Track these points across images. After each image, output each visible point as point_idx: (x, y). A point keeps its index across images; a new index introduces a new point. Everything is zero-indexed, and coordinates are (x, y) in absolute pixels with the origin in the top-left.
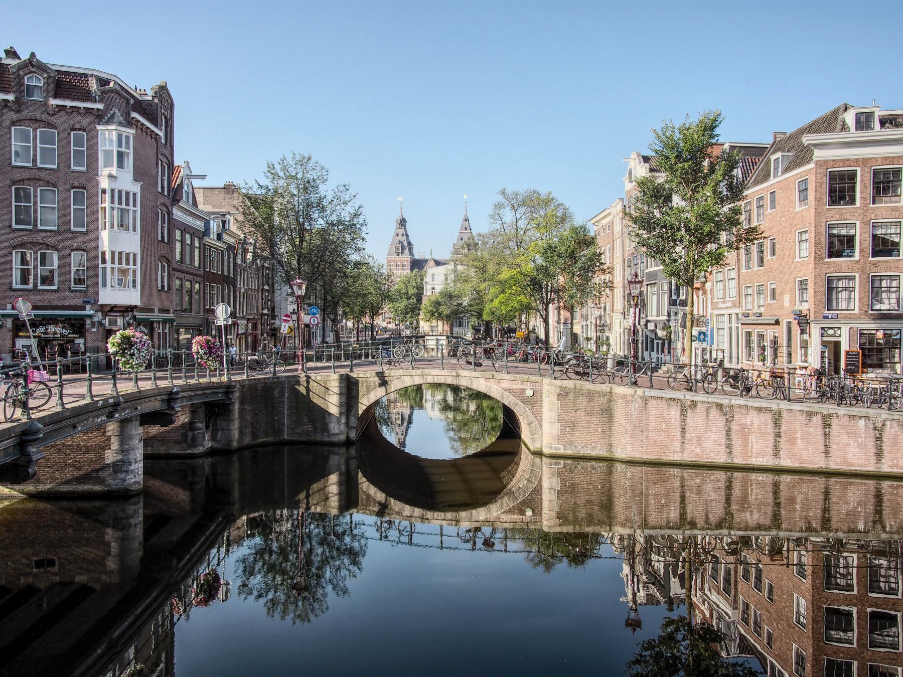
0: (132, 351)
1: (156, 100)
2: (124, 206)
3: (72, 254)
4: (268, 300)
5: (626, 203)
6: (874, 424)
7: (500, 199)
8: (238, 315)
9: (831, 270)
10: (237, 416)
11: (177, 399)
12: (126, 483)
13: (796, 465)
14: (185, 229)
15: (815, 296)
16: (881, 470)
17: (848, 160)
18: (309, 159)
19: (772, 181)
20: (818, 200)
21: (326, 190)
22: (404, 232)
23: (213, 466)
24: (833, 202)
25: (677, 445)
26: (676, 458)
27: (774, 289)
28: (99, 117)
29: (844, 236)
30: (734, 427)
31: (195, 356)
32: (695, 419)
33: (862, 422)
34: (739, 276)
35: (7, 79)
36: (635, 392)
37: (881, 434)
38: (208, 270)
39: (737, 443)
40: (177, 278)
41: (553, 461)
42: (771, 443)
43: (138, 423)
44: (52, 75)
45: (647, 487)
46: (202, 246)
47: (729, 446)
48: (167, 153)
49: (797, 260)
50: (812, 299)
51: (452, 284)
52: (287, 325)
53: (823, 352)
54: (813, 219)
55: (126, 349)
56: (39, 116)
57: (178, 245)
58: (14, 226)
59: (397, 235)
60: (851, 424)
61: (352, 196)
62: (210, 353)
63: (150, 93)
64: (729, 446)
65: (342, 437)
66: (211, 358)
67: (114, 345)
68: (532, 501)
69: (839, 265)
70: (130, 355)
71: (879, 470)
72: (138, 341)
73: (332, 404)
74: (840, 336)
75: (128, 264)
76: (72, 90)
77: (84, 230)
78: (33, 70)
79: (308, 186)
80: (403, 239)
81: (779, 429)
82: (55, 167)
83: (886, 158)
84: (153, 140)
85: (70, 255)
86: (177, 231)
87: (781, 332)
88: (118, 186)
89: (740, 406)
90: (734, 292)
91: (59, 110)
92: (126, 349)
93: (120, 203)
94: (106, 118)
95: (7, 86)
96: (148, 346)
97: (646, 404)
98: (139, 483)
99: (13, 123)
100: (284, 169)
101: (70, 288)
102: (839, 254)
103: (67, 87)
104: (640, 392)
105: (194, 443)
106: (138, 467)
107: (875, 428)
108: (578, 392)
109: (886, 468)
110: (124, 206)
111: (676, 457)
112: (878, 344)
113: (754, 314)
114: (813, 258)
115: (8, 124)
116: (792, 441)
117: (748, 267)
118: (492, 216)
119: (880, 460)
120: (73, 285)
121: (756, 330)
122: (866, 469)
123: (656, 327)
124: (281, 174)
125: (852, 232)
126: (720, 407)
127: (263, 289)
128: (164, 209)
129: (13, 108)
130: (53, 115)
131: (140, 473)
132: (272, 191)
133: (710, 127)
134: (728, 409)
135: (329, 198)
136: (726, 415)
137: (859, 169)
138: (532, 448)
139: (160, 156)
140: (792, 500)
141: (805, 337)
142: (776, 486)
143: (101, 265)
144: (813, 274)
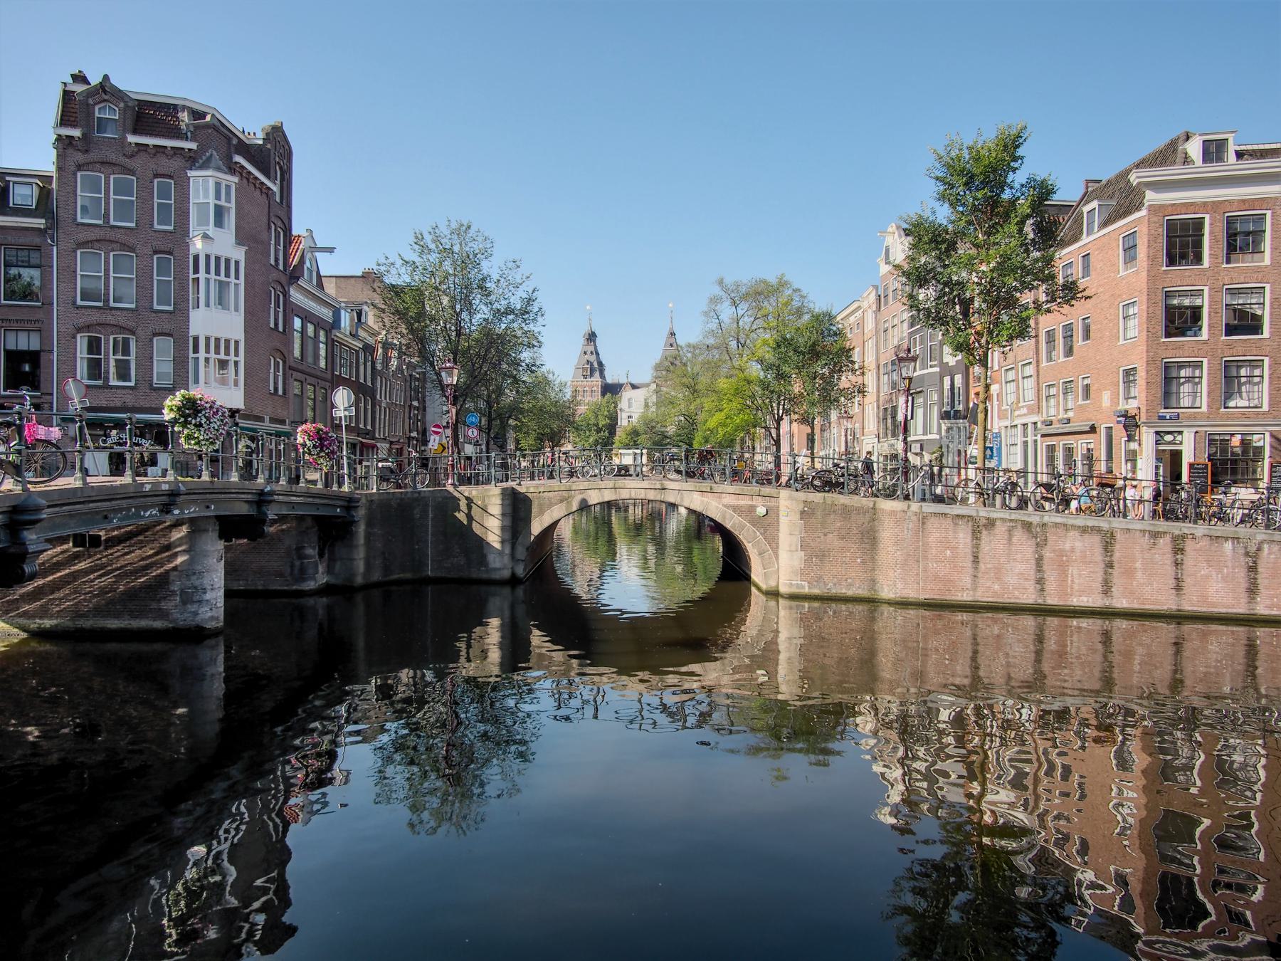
0: (198, 419)
1: (269, 146)
2: (222, 278)
3: (155, 339)
4: (418, 420)
5: (881, 292)
6: (1246, 548)
7: (717, 291)
8: (377, 435)
9: (1169, 354)
10: (362, 541)
11: (271, 502)
12: (198, 618)
13: (1135, 605)
14: (307, 317)
15: (1147, 388)
16: (1256, 612)
17: (1192, 204)
18: (469, 227)
19: (1085, 239)
20: (1152, 259)
21: (491, 268)
22: (593, 350)
23: (329, 608)
24: (1171, 261)
25: (967, 580)
26: (965, 598)
27: (1088, 386)
28: (192, 160)
29: (1187, 308)
30: (1048, 554)
31: (301, 450)
32: (992, 544)
33: (1228, 545)
34: (1038, 371)
35: (73, 110)
36: (909, 507)
37: (1255, 562)
38: (338, 373)
39: (1051, 576)
40: (296, 380)
41: (794, 604)
42: (1099, 576)
43: (216, 534)
44: (130, 104)
45: (925, 637)
46: (329, 343)
47: (1040, 581)
48: (282, 214)
49: (1122, 342)
50: (1144, 394)
51: (653, 409)
52: (437, 438)
53: (1157, 468)
54: (1144, 286)
55: (189, 415)
56: (112, 157)
57: (297, 336)
58: (79, 302)
59: (585, 353)
60: (1213, 548)
61: (524, 277)
62: (322, 446)
63: (260, 135)
64: (1040, 581)
65: (506, 574)
66: (322, 454)
67: (172, 410)
68: (767, 656)
69: (1180, 347)
70: (195, 425)
71: (1252, 612)
72: (208, 405)
73: (492, 529)
74: (1181, 443)
75: (227, 353)
76: (156, 125)
77: (171, 308)
78: (106, 97)
79: (467, 262)
80: (593, 358)
81: (1111, 556)
82: (133, 225)
83: (1243, 201)
84: (264, 196)
85: (151, 340)
86: (296, 318)
87: (1098, 444)
88: (214, 251)
89: (1056, 525)
90: (1030, 395)
91: (139, 150)
92: (189, 415)
93: (218, 273)
94: (201, 161)
95: (72, 119)
96: (223, 415)
97: (923, 523)
98: (217, 619)
99: (79, 167)
100: (437, 240)
101: (151, 384)
102: (1182, 333)
103: (151, 120)
104: (915, 506)
105: (302, 575)
106: (216, 596)
107: (1247, 554)
108: (830, 510)
109: (1262, 609)
110: (222, 278)
111: (965, 597)
112: (1233, 454)
113: (1060, 421)
114: (1145, 337)
115: (73, 168)
116: (1130, 573)
117: (1050, 359)
118: (706, 314)
119: (1254, 598)
120: (155, 381)
121: (1060, 443)
122: (1234, 611)
123: (922, 449)
124: (432, 246)
125: (1198, 302)
126: (1027, 526)
127: (410, 406)
128: (279, 288)
129: (80, 147)
130: (131, 156)
131: (219, 605)
132: (420, 268)
133: (1011, 146)
134: (1038, 529)
135: (495, 277)
136: (1036, 538)
137: (1207, 217)
138: (764, 587)
139: (273, 219)
140: (1128, 655)
141: (1133, 446)
142: (1106, 637)
143: (191, 355)
144: (1145, 359)
